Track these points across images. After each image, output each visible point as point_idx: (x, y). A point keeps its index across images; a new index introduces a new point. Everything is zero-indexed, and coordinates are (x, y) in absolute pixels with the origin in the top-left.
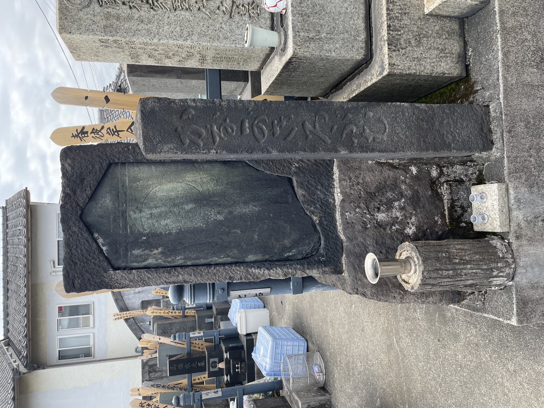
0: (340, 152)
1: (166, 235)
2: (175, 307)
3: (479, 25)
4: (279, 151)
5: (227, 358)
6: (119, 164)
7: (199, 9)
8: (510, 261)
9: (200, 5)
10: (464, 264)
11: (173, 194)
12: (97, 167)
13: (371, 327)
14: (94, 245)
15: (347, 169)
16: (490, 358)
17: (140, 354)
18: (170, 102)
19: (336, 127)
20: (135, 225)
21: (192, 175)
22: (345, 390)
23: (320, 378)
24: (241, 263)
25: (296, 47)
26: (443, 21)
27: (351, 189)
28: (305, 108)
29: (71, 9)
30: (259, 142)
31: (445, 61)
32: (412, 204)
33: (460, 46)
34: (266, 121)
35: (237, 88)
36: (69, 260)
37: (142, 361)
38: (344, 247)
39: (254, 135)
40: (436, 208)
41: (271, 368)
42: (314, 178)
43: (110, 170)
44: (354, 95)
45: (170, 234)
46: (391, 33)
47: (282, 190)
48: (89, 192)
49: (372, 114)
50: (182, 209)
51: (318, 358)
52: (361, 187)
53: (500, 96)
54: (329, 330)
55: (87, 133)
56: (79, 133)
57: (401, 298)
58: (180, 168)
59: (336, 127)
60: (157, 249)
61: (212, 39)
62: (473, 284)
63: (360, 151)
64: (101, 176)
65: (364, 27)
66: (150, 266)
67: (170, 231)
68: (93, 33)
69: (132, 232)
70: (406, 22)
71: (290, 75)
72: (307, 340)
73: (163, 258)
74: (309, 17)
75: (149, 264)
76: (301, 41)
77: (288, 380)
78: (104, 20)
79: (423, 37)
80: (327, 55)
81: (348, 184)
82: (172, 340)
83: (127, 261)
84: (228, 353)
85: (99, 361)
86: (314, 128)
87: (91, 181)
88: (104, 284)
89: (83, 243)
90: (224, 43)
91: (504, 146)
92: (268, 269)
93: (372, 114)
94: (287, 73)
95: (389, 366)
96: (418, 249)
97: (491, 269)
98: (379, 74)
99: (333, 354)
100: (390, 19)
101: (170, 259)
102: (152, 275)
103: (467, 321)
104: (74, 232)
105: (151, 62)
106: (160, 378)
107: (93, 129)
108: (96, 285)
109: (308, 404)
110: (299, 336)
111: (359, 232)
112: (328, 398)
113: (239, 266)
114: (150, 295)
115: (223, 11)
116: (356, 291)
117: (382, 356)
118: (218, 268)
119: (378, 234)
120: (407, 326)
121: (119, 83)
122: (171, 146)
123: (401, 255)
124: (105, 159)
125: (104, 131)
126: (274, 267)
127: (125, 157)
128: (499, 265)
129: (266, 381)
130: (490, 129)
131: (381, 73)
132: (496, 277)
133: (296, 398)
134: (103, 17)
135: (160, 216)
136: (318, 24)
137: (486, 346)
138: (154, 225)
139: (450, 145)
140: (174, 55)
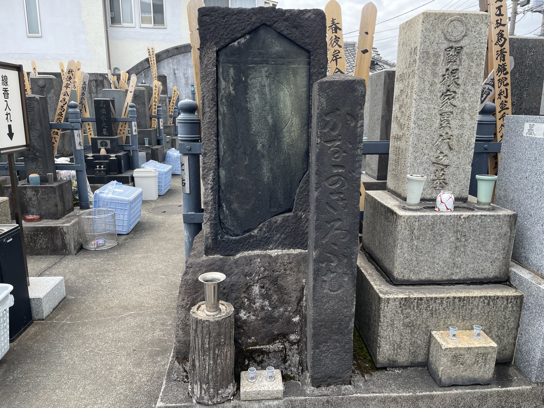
0: (315, 250)
2: (161, 108)
3: (421, 378)
4: (317, 198)
5: (111, 157)
6: (309, 60)
7: (441, 136)
8: (215, 400)
9: (444, 136)
10: (214, 358)
11: (282, 106)
12: (307, 40)
13: (144, 292)
14: (240, 35)
16: (120, 393)
18: (362, 105)
19: (336, 248)
20: (256, 71)
26: (425, 347)
27: (281, 263)
28: (353, 221)
29: (444, 24)
30: (325, 180)
31: (390, 349)
32: (267, 317)
33: (403, 362)
35: (372, 170)
36: (227, 12)
40: (262, 338)
41: (102, 198)
43: (304, 52)
44: (363, 271)
45: (247, 102)
46: (416, 301)
47: (282, 203)
48: (285, 33)
49: (346, 280)
51: (111, 243)
53: (359, 394)
55: (336, 32)
56: (335, 25)
57: (183, 305)
58: (304, 113)
59: (336, 248)
60: (233, 90)
61: (415, 146)
62: (195, 367)
63: (314, 269)
64: (299, 43)
65: (421, 279)
66: (219, 83)
68: (423, 42)
70: (424, 314)
71: (382, 215)
72: (128, 234)
74: (432, 230)
75: (221, 82)
77: (90, 214)
79: (411, 330)
80: (398, 246)
82: (130, 104)
84: (115, 158)
85: (107, 31)
86: (336, 229)
87: (295, 34)
88: (205, 42)
89: (241, 25)
92: (212, 188)
93: (346, 280)
94: (384, 211)
95: (107, 307)
96: (228, 317)
97: (208, 383)
98: (380, 291)
100: (427, 300)
101: (224, 100)
103: (154, 374)
104: (251, 18)
105: (396, 92)
106: (90, 91)
107: (339, 38)
108: (204, 35)
110: (132, 227)
111: (243, 270)
112: (72, 252)
113: (215, 162)
114: (172, 84)
115: (439, 157)
116: (190, 266)
117: (116, 302)
118: (215, 143)
119: (241, 286)
120: (147, 324)
121: (380, 64)
122: (324, 105)
123: (222, 304)
125: (337, 48)
126: (213, 193)
127: (315, 65)
128: (212, 390)
129: (89, 194)
130: (331, 385)
131: (381, 292)
132: (201, 387)
133: (73, 221)
134: (436, 51)
135: (262, 94)
136: (425, 238)
137: (131, 389)
138: (255, 88)
139: (317, 349)
140: (402, 112)
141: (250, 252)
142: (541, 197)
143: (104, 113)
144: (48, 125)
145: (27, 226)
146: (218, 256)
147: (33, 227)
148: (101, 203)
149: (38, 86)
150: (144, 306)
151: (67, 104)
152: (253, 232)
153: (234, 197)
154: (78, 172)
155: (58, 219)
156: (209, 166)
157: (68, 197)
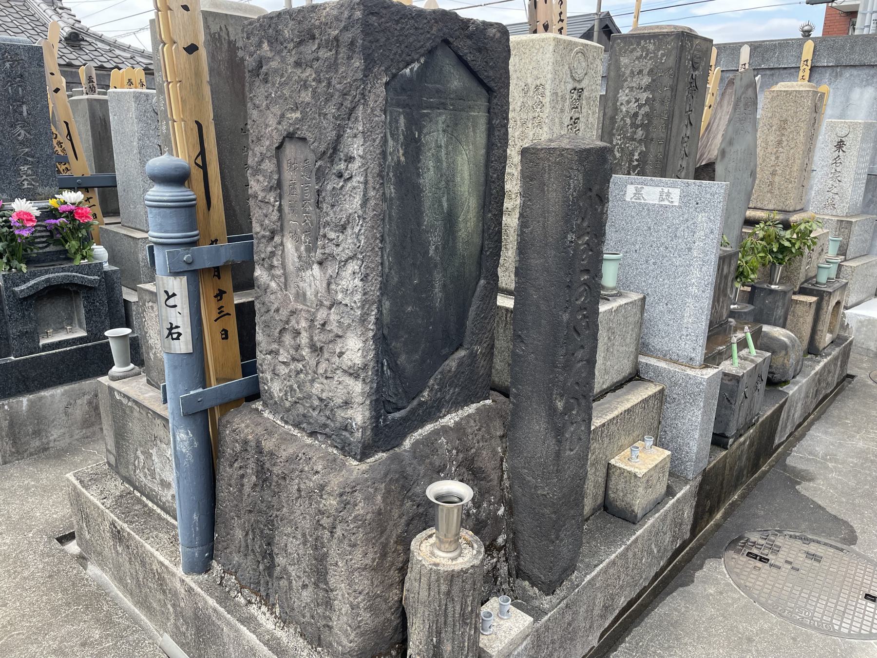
11: (459, 179)
12: (491, 73)
36: (403, 12)
48: (469, 58)
91: (556, 607)
92: (374, 336)
104: (431, 28)
135: (438, 160)
142: (661, 272)
146: (381, 456)
152: (423, 396)
156: (371, 297)
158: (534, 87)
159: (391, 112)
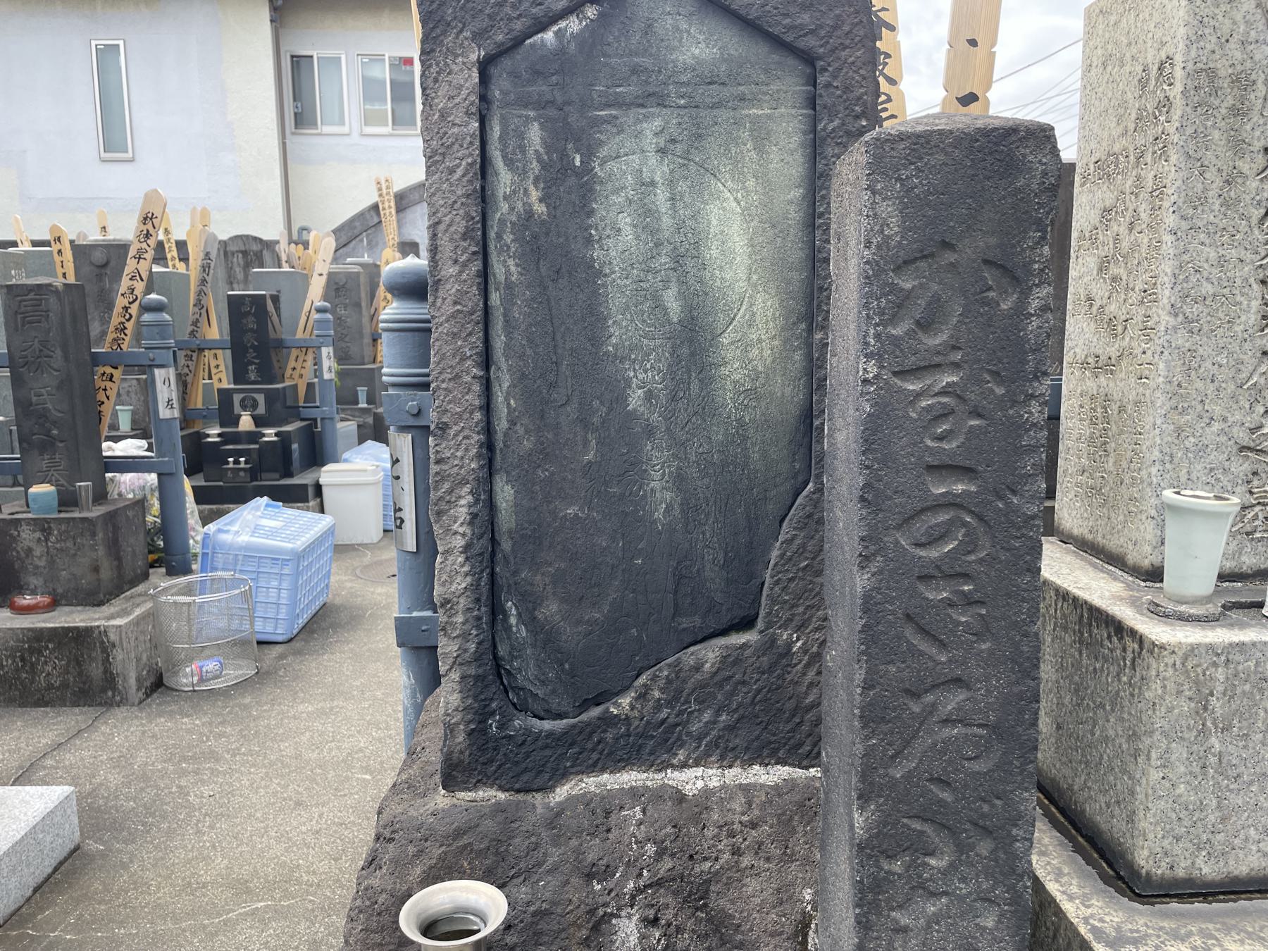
0: (862, 809)
1: (586, 230)
4: (867, 597)
5: (264, 435)
6: (810, 88)
11: (715, 252)
12: (805, 18)
13: (304, 829)
15: (784, 814)
17: (295, 237)
19: (946, 796)
21: (770, 314)
22: (144, 747)
23: (186, 676)
24: (491, 461)
25: (1180, 653)
27: (720, 827)
30: (899, 527)
34: (969, 553)
37: (278, 242)
38: (529, 797)
39: (923, 510)
41: (222, 545)
42: (753, 703)
43: (791, 61)
45: (589, 241)
47: (718, 597)
49: (990, 923)
50: (666, 281)
52: (727, 862)
54: (310, 703)
59: (946, 796)
60: (541, 201)
61: (1176, 392)
63: (861, 882)
64: (775, 30)
65: (1236, 873)
67: (598, 242)
69: (597, 123)
71: (1065, 628)
72: (290, 640)
73: (514, 219)
75: (497, 174)
76: (1199, 670)
77: (188, 590)
78: (1230, 71)
80: (1154, 755)
81: (737, 818)
82: (318, 304)
83: (507, 105)
84: (275, 439)
85: (284, 144)
86: (946, 722)
90: (1164, 426)
92: (467, 548)
93: (990, 923)
99: (244, 714)
101: (508, 238)
102: (459, 179)
106: (230, 277)
109: (117, 643)
110: (301, 622)
113: (479, 456)
116: (387, 833)
117: (220, 863)
118: (476, 387)
119: (571, 918)
122: (894, 228)
124: (828, 42)
126: (473, 567)
127: (834, 105)
129: (192, 533)
133: (138, 612)
134: (1239, 68)
136: (1249, 727)
138: (617, 191)
141: (606, 776)
143: (251, 326)
144: (88, 358)
145: (14, 626)
146: (491, 795)
147: (29, 630)
148: (220, 560)
149: (92, 264)
150: (298, 881)
151: (138, 302)
153: (547, 580)
154: (162, 477)
155: (100, 604)
157: (134, 545)
158: (1156, 68)
159: (503, 118)
